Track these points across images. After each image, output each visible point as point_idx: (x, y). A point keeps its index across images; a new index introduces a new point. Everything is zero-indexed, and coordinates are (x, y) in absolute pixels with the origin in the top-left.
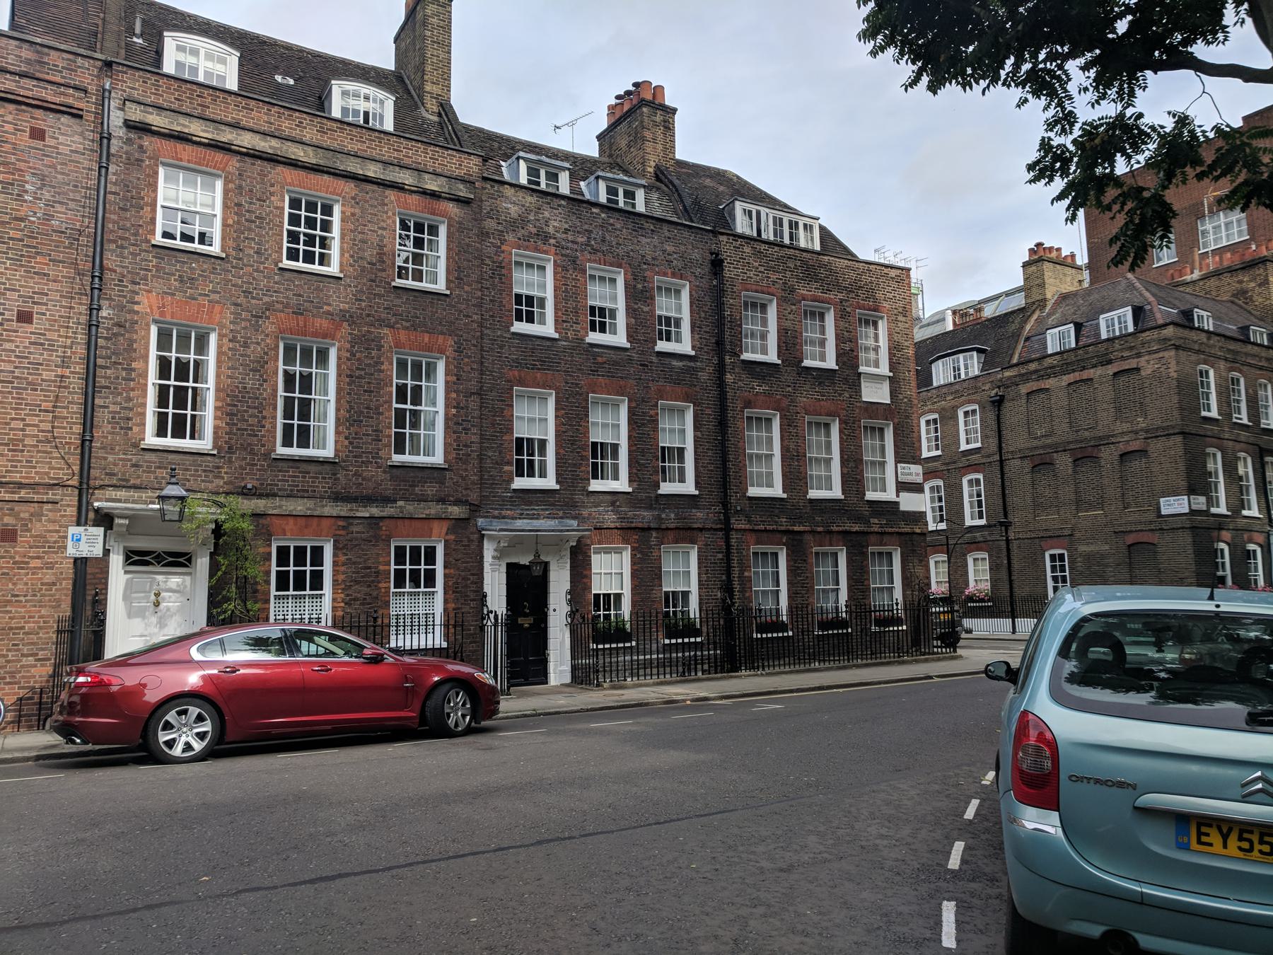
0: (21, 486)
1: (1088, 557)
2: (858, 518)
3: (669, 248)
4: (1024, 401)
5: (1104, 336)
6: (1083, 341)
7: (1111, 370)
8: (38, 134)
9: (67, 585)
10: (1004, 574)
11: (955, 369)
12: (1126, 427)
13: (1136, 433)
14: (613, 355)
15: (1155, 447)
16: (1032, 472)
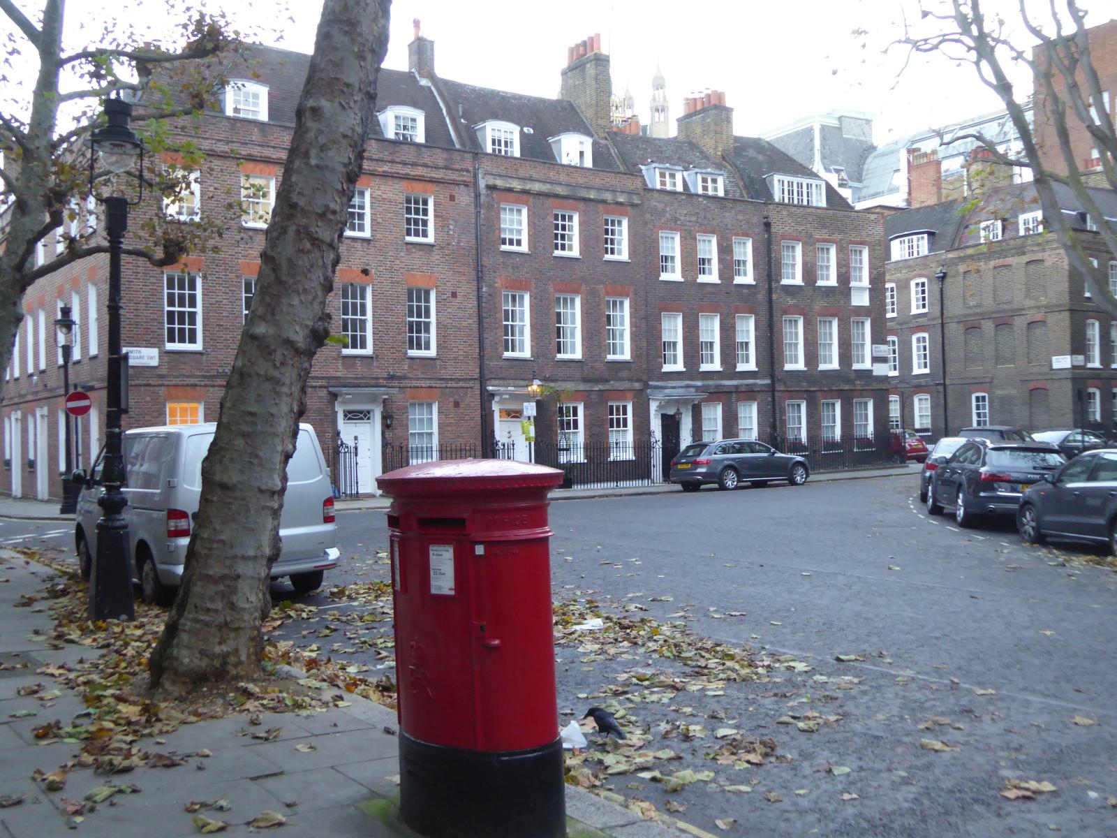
0: (460, 380)
1: (1003, 400)
2: (849, 381)
3: (740, 217)
4: (961, 278)
5: (1022, 233)
6: (1007, 236)
7: (1025, 259)
8: (452, 198)
9: (479, 428)
10: (941, 411)
11: (911, 247)
12: (1032, 303)
13: (1038, 307)
14: (712, 290)
15: (1052, 319)
16: (965, 333)
